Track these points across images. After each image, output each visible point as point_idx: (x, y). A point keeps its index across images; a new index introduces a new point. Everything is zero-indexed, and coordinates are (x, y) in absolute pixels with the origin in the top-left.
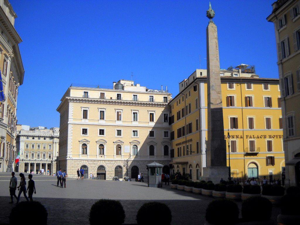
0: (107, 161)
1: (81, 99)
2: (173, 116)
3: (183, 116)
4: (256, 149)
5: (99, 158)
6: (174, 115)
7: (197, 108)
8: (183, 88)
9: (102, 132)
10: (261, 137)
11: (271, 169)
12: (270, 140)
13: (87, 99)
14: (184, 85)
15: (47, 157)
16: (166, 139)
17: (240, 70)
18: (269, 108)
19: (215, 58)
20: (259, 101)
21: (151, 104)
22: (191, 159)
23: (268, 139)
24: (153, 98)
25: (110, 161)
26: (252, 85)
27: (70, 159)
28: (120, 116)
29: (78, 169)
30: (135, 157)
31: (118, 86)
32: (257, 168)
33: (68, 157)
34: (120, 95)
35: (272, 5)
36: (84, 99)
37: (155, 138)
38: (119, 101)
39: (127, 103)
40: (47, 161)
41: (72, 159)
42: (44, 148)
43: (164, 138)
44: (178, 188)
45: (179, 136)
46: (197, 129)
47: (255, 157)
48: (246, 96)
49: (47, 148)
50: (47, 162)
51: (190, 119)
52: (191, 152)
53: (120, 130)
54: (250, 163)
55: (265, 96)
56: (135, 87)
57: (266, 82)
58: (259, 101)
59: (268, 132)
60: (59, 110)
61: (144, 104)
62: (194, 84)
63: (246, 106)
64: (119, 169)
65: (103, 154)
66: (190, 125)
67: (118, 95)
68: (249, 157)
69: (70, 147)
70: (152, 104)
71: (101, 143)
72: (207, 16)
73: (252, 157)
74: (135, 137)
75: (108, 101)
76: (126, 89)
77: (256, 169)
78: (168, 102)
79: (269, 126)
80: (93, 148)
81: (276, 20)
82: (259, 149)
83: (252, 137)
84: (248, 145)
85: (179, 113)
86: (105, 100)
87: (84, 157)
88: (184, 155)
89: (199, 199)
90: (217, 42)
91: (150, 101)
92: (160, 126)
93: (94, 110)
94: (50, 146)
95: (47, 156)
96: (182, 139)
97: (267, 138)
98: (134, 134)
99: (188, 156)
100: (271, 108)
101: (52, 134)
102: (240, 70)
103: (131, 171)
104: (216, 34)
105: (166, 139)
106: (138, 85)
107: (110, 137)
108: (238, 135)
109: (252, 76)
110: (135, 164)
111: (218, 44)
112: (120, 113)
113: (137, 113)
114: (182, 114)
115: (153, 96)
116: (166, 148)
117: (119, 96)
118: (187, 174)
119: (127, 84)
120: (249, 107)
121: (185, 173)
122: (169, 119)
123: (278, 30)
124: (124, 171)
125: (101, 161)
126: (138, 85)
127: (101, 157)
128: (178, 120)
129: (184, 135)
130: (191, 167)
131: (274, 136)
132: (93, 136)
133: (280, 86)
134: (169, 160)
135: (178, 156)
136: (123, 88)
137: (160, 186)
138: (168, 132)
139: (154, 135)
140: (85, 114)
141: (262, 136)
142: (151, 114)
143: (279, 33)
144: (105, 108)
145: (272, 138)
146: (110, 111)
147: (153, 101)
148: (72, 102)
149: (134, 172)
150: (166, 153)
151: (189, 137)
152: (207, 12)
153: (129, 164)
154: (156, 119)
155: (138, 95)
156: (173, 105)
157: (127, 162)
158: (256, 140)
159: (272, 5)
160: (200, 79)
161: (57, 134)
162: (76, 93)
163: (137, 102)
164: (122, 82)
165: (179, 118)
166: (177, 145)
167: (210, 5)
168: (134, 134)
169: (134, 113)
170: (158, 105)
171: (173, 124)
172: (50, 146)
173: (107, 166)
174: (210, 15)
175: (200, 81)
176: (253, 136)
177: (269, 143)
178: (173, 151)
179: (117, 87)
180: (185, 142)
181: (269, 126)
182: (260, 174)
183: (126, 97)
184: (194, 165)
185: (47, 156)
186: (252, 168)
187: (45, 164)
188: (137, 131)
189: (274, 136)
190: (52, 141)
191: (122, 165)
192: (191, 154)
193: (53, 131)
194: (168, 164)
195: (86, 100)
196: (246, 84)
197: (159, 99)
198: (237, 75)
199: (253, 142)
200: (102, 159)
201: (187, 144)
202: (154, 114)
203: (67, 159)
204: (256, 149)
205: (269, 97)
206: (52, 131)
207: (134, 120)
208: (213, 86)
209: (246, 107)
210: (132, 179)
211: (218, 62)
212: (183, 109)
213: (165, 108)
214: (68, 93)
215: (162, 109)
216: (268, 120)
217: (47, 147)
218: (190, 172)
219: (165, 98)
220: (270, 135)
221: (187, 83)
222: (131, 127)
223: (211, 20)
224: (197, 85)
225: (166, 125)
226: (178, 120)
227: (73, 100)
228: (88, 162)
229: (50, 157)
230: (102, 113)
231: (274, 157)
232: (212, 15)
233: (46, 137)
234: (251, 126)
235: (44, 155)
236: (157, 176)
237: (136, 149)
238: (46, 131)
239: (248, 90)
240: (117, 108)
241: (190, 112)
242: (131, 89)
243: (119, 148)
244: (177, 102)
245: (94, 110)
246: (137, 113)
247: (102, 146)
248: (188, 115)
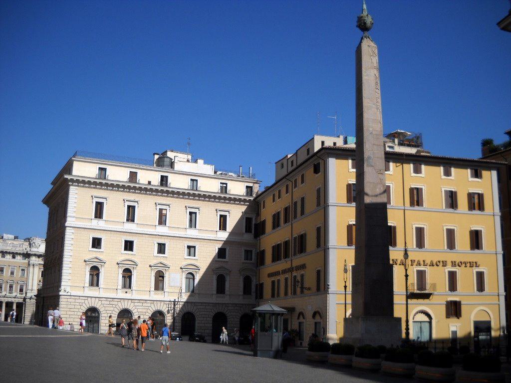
0: (137, 301)
1: (92, 180)
2: (264, 222)
4: (428, 286)
5: (121, 294)
6: (265, 221)
7: (318, 204)
9: (129, 246)
10: (438, 263)
11: (454, 324)
12: (453, 269)
13: (104, 182)
15: (16, 291)
17: (396, 141)
18: (451, 210)
19: (374, 106)
20: (434, 198)
21: (223, 197)
22: (305, 304)
23: (450, 268)
25: (142, 301)
26: (423, 167)
27: (67, 294)
28: (164, 218)
29: (139, 317)
30: (190, 296)
31: (163, 162)
32: (430, 323)
33: (62, 291)
34: (167, 177)
36: (98, 181)
37: (227, 262)
39: (178, 193)
40: (15, 297)
41: (69, 294)
42: (12, 273)
43: (245, 261)
45: (276, 258)
46: (318, 246)
47: (426, 301)
48: (412, 186)
49: (18, 274)
50: (16, 299)
52: (302, 288)
53: (163, 243)
54: (417, 313)
55: (446, 189)
56: (194, 164)
57: (447, 163)
58: (434, 198)
59: (450, 256)
60: (47, 201)
61: (210, 197)
62: (316, 162)
63: (412, 204)
64: (159, 318)
65: (130, 287)
66: (302, 238)
67: (162, 177)
68: (414, 301)
69: (68, 272)
71: (127, 267)
73: (421, 301)
75: (143, 187)
76: (177, 167)
77: (427, 325)
78: (254, 195)
79: (451, 245)
80: (111, 276)
82: (434, 286)
83: (422, 263)
84: (413, 279)
85: (276, 217)
86: (137, 186)
87: (93, 292)
88: (286, 294)
90: (377, 75)
91: (222, 192)
92: (237, 239)
93: (115, 204)
94: (23, 270)
95: (16, 288)
96: (282, 265)
97: (447, 267)
100: (456, 211)
101: (28, 249)
103: (180, 321)
104: (375, 60)
106: (200, 162)
107: (144, 256)
109: (418, 151)
110: (190, 309)
111: (380, 79)
112: (164, 212)
113: (196, 213)
115: (226, 184)
116: (247, 281)
117: (164, 180)
119: (181, 161)
120: (416, 208)
122: (255, 226)
124: (169, 320)
125: (93, 299)
126: (200, 162)
127: (126, 292)
129: (286, 256)
130: (301, 317)
132: (112, 255)
135: (273, 296)
136: (172, 164)
137: (278, 355)
139: (225, 256)
140: (99, 211)
141: (439, 262)
142: (221, 216)
144: (136, 200)
145: (457, 267)
146: (147, 207)
147: (226, 192)
148: (76, 186)
150: (247, 290)
151: (297, 261)
154: (231, 224)
156: (264, 202)
157: (174, 305)
158: (428, 270)
160: (328, 151)
161: (42, 249)
162: (83, 169)
163: (197, 193)
164: (170, 154)
166: (270, 275)
167: (365, 7)
169: (191, 213)
170: (235, 200)
172: (23, 270)
173: (136, 310)
174: (365, 23)
176: (424, 261)
177: (452, 276)
178: (260, 287)
179: (160, 163)
180: (290, 270)
181: (451, 245)
182: (434, 336)
183: (177, 182)
184: (309, 314)
185: (16, 288)
186: (421, 322)
187: (12, 303)
188: (194, 247)
189: (461, 262)
190: (26, 261)
191: (164, 309)
192: (302, 292)
193: (30, 244)
195: (101, 182)
196: (412, 165)
197: (237, 188)
200: (128, 296)
201: (294, 274)
202: (228, 217)
203: (60, 293)
204: (447, 286)
206: (27, 244)
207: (191, 226)
208: (369, 158)
210: (183, 338)
211: (378, 113)
213: (249, 207)
214: (68, 168)
215: (243, 208)
216: (451, 233)
217: (18, 272)
218: (300, 326)
219: (249, 189)
220: (453, 260)
223: (366, 33)
225: (248, 237)
227: (78, 181)
228: (100, 302)
229: (21, 290)
230: (131, 210)
233: (17, 254)
234: (420, 243)
235: (11, 287)
236: (274, 334)
237: (191, 280)
238: (16, 243)
240: (159, 202)
241: (302, 213)
242: (186, 169)
243: (160, 277)
244: (274, 195)
245: (115, 204)
246: (196, 213)
247: (127, 274)
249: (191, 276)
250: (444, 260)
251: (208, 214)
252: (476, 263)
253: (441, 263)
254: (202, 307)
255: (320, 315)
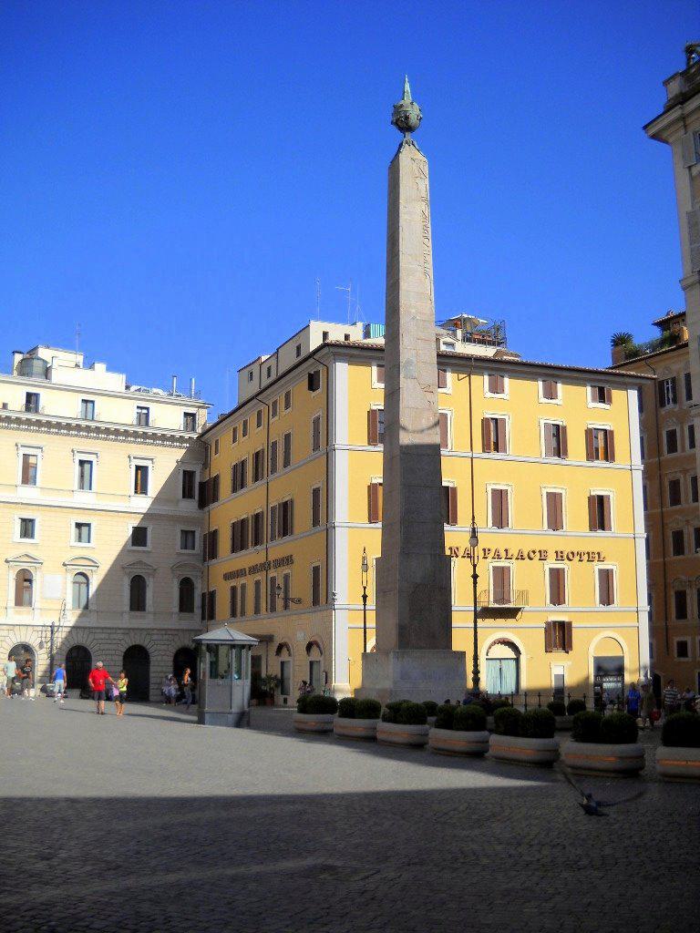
3: (256, 478)
6: (217, 477)
7: (316, 447)
8: (254, 388)
12: (559, 565)
14: (256, 375)
16: (186, 557)
17: (459, 332)
18: (555, 459)
19: (419, 268)
20: (525, 437)
21: (142, 432)
22: (293, 628)
23: (552, 563)
24: (147, 415)
26: (506, 380)
30: (81, 616)
32: (517, 660)
34: (37, 395)
35: (666, 83)
37: (149, 552)
38: (33, 417)
43: (184, 551)
44: (380, 736)
45: (239, 544)
46: (316, 522)
47: (511, 622)
51: (285, 486)
52: (286, 599)
54: (495, 643)
58: (525, 437)
59: (553, 542)
61: (117, 432)
63: (486, 448)
66: (286, 508)
67: (29, 395)
68: (489, 622)
70: (145, 435)
72: (396, 123)
73: (500, 622)
74: (80, 544)
76: (56, 376)
78: (199, 430)
79: (555, 521)
81: (683, 131)
83: (503, 554)
84: (487, 582)
85: (239, 470)
88: (257, 611)
89: (545, 784)
92: (166, 509)
96: (251, 557)
98: (80, 534)
99: (274, 614)
100: (564, 462)
102: (459, 332)
104: (424, 185)
105: (189, 555)
106: (100, 367)
108: (458, 545)
112: (32, 460)
114: (257, 467)
116: (186, 586)
117: (32, 400)
118: (269, 678)
119: (63, 363)
121: (260, 675)
123: (690, 168)
124: (41, 662)
126: (100, 367)
128: (234, 490)
129: (257, 542)
131: (573, 553)
133: (593, 393)
134: (197, 627)
135: (233, 614)
136: (47, 372)
137: (242, 721)
138: (193, 532)
141: (534, 552)
142: (138, 468)
143: (692, 179)
145: (566, 561)
147: (147, 424)
149: (77, 668)
150: (185, 604)
151: (278, 548)
152: (398, 109)
153: (60, 640)
154: (156, 483)
155: (98, 400)
158: (514, 566)
159: (666, 83)
160: (336, 350)
163: (93, 425)
164: (43, 353)
165: (238, 483)
166: (227, 577)
167: (407, 87)
168: (80, 534)
169: (82, 463)
171: (212, 506)
175: (335, 354)
176: (506, 551)
177: (557, 577)
178: (210, 599)
179: (25, 369)
180: (265, 567)
181: (555, 521)
182: (524, 684)
183: (56, 405)
186: (500, 659)
189: (573, 553)
191: (33, 640)
192: (286, 607)
194: (187, 642)
197: (168, 417)
198: (452, 345)
199: (506, 573)
201: (272, 573)
205: (558, 426)
207: (82, 487)
208: (409, 363)
209: (484, 451)
212: (257, 455)
216: (554, 501)
220: (559, 549)
221: (269, 369)
222: (82, 511)
223: (409, 136)
224: (321, 369)
225: (189, 507)
226: (234, 490)
231: (570, 624)
232: (413, 120)
237: (83, 587)
239: (493, 395)
241: (287, 463)
242: (73, 380)
243: (26, 580)
244: (235, 430)
246: (90, 462)
248: (276, 475)
249: (82, 579)
250: (543, 549)
251: (115, 464)
252: (599, 553)
253: (538, 554)
254: (103, 636)
255: (318, 647)
